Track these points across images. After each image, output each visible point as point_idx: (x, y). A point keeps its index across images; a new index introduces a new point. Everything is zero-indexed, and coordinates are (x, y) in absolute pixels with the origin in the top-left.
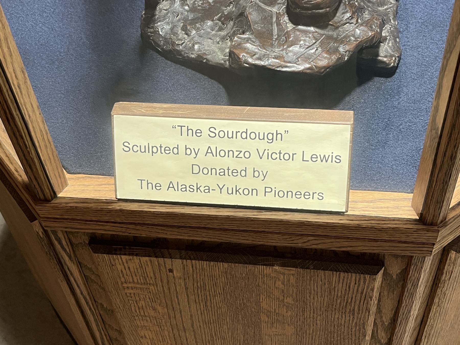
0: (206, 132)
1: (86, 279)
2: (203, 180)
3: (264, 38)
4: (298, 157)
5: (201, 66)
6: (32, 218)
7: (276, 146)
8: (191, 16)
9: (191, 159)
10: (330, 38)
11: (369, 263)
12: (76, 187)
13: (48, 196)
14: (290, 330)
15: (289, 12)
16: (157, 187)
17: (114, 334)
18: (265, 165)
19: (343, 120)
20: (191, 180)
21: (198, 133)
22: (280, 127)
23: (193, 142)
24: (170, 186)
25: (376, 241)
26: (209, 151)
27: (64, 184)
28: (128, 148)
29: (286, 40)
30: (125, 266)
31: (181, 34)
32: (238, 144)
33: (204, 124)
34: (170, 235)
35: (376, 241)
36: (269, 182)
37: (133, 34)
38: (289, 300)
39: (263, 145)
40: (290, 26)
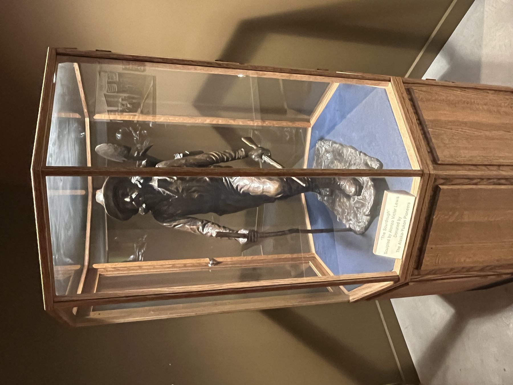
0: (384, 231)
1: (434, 274)
2: (399, 235)
3: (363, 205)
4: (396, 208)
5: (370, 222)
6: (407, 284)
7: (391, 213)
8: (356, 219)
9: (392, 237)
10: (366, 187)
11: (436, 190)
12: (397, 270)
13: (397, 277)
14: (466, 213)
15: (358, 196)
16: (399, 247)
17: (465, 270)
18: (397, 217)
19: (387, 195)
20: (398, 238)
21: (384, 233)
22: (386, 211)
23: (387, 235)
24: (400, 244)
25: (426, 189)
26: (390, 231)
27: (395, 272)
28: (386, 253)
29: (364, 199)
30: (428, 261)
31: (360, 224)
32: (389, 224)
33: (382, 232)
34: (417, 245)
35: (426, 189)
36: (402, 217)
37: (360, 237)
38: (450, 213)
39: (390, 217)
40: (361, 196)
